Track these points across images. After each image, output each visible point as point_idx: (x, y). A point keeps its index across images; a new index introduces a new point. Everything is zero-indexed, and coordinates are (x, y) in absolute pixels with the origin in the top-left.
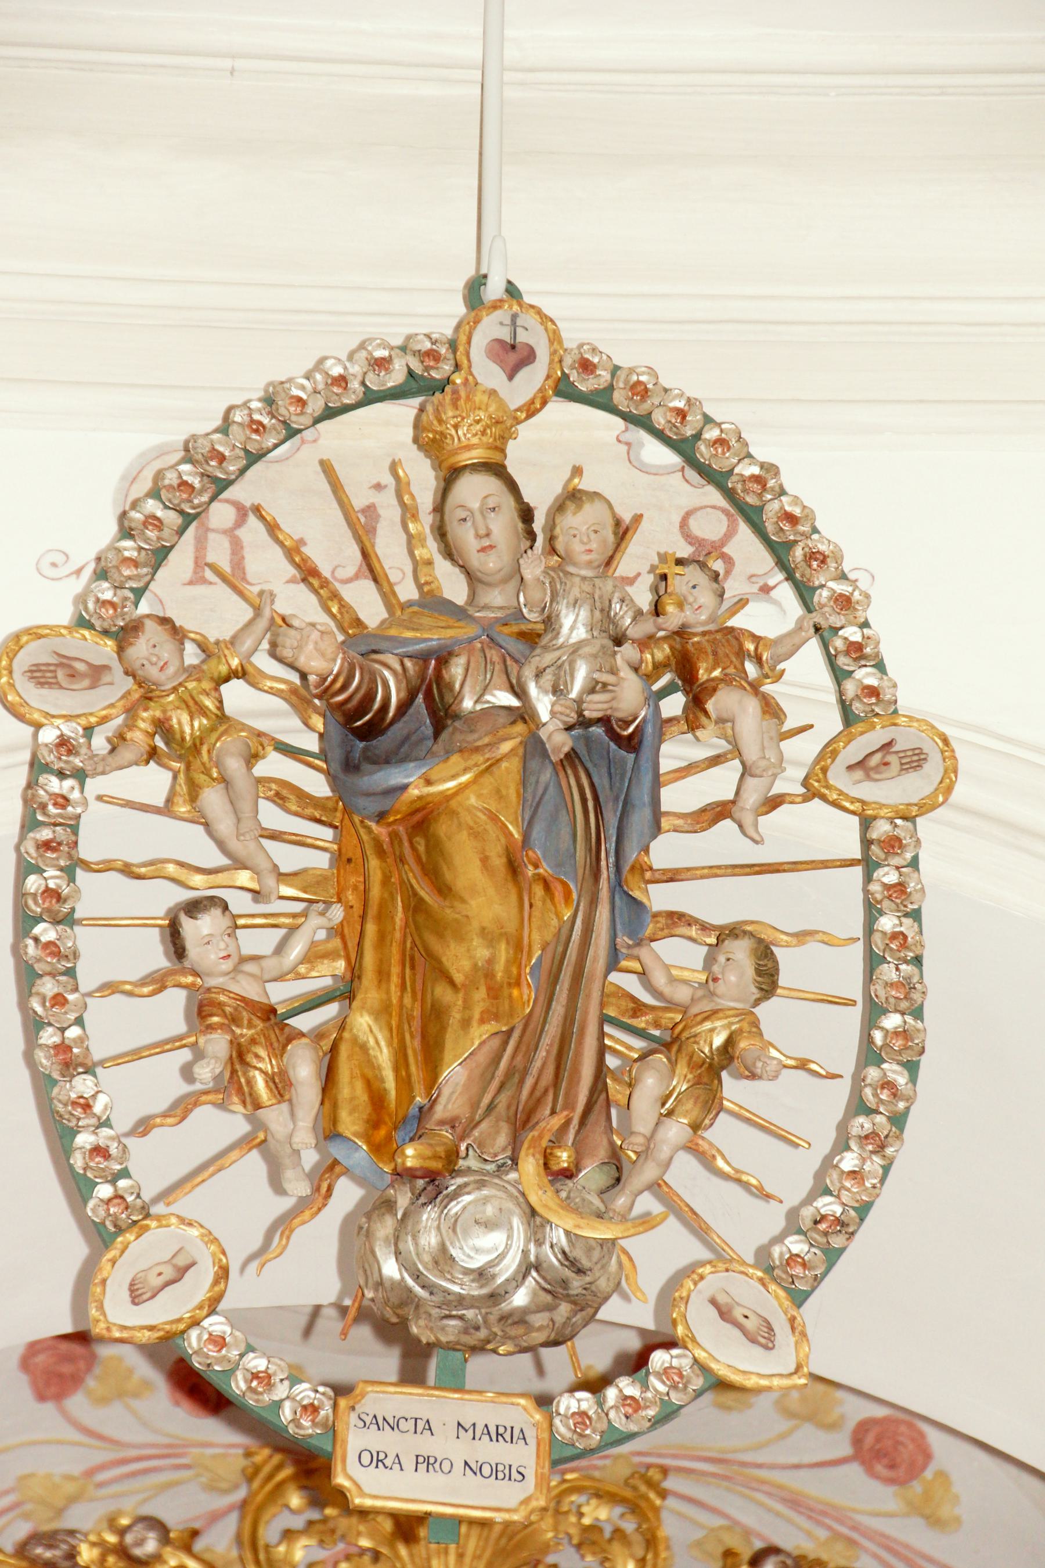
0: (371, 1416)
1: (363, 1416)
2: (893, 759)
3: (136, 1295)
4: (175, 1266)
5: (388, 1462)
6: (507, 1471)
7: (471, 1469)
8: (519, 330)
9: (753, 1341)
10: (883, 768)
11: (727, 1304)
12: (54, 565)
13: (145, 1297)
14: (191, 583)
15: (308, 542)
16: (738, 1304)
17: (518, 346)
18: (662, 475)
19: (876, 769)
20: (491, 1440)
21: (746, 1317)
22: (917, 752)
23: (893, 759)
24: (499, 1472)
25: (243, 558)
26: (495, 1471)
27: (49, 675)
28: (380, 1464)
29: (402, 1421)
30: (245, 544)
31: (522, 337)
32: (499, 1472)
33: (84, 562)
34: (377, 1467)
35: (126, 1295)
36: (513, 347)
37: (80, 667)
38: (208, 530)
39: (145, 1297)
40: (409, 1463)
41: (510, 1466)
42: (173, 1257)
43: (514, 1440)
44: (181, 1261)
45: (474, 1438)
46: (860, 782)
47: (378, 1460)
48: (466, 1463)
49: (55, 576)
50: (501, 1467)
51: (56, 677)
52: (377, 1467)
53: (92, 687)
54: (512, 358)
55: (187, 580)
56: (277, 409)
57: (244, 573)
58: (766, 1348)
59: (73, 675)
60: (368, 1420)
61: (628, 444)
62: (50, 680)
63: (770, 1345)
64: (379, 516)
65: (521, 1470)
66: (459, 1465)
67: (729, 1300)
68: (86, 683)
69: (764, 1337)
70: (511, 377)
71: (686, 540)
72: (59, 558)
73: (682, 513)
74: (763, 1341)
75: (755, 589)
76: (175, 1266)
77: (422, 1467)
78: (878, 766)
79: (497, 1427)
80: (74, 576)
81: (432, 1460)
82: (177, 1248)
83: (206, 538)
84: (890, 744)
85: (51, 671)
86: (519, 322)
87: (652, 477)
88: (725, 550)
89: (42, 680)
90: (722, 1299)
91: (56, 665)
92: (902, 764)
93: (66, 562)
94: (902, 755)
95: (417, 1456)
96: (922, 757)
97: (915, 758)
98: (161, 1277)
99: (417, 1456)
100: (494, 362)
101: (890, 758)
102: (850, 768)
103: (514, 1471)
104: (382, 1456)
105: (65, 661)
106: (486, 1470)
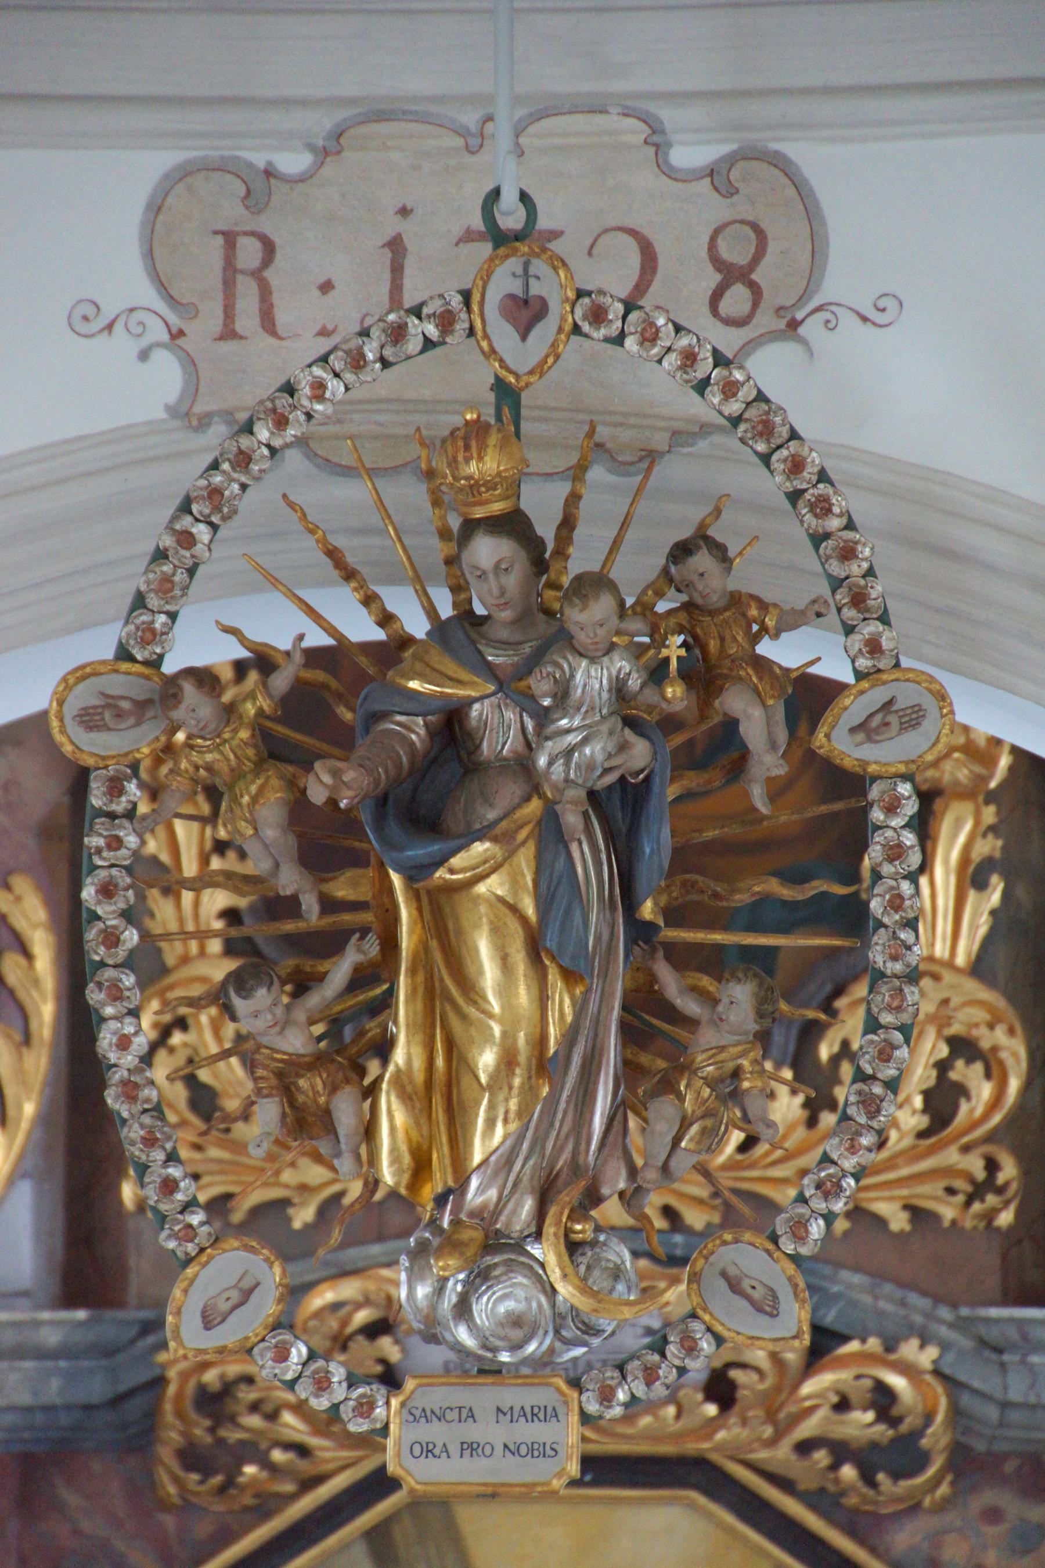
0: (420, 1410)
1: (414, 1411)
2: (893, 719)
3: (209, 1320)
4: (241, 1290)
5: (437, 1452)
6: (541, 1449)
7: (510, 1451)
8: (532, 281)
9: (760, 1310)
10: (884, 729)
11: (736, 1276)
12: (85, 318)
13: (216, 1322)
14: (221, 338)
15: (336, 284)
16: (747, 1276)
17: (531, 302)
18: (691, 181)
19: (877, 730)
20: (527, 1421)
21: (754, 1288)
22: (916, 709)
23: (893, 719)
24: (537, 1450)
25: (272, 305)
26: (531, 1450)
27: (97, 718)
28: (430, 1455)
29: (448, 1411)
30: (274, 289)
31: (536, 289)
32: (537, 1450)
33: (113, 316)
34: (427, 1457)
35: (198, 1322)
36: (526, 302)
37: (126, 705)
38: (236, 271)
39: (216, 1322)
40: (454, 1449)
41: (545, 1407)
42: (240, 1280)
43: (548, 1418)
44: (246, 1284)
45: (512, 1421)
46: (862, 743)
47: (428, 1451)
48: (506, 1446)
49: (88, 333)
50: (536, 1446)
51: (103, 719)
52: (427, 1457)
53: (138, 723)
54: (525, 315)
55: (217, 335)
56: (299, 400)
57: (274, 325)
58: (771, 1315)
59: (119, 715)
60: (417, 1413)
61: (657, 146)
62: (98, 723)
63: (775, 1312)
64: (406, 249)
65: (555, 1446)
66: (499, 1449)
67: (738, 1273)
68: (132, 721)
69: (769, 1306)
70: (524, 337)
71: (714, 266)
72: (90, 310)
73: (709, 232)
74: (768, 1309)
75: (782, 324)
76: (241, 1290)
77: (467, 1453)
78: (878, 727)
79: (532, 1407)
80: (106, 332)
81: (475, 1446)
82: (243, 1271)
83: (234, 283)
84: (890, 702)
85: (100, 714)
86: (532, 270)
87: (679, 185)
88: (754, 277)
89: (91, 724)
90: (732, 1271)
91: (103, 707)
92: (901, 724)
93: (97, 315)
94: (901, 714)
95: (462, 1443)
96: (921, 713)
97: (914, 716)
98: (230, 1301)
99: (462, 1443)
100: (508, 321)
101: (890, 718)
102: (853, 730)
103: (548, 1448)
104: (431, 1447)
105: (110, 701)
106: (523, 1450)
